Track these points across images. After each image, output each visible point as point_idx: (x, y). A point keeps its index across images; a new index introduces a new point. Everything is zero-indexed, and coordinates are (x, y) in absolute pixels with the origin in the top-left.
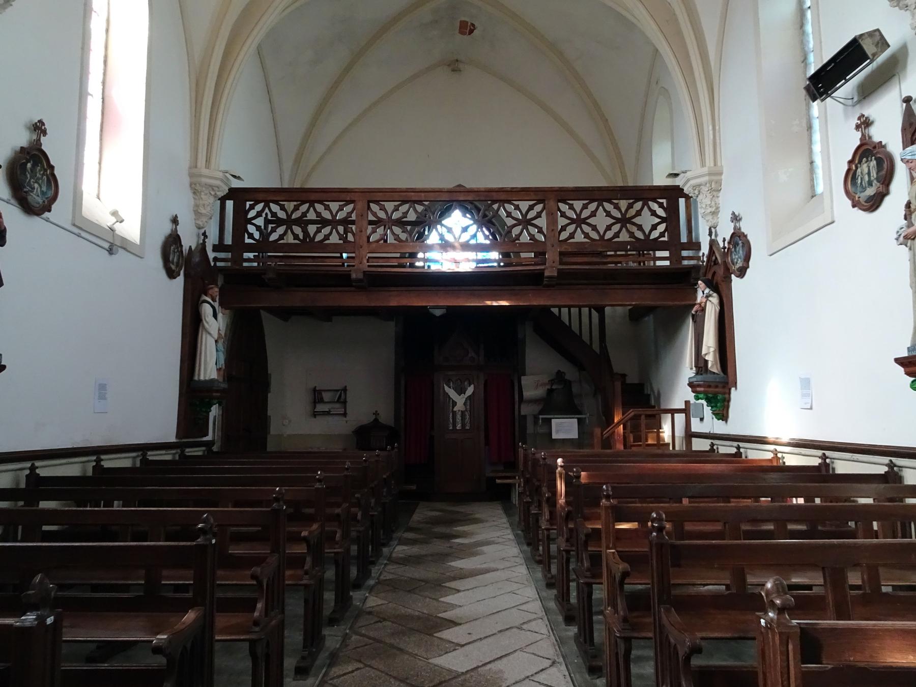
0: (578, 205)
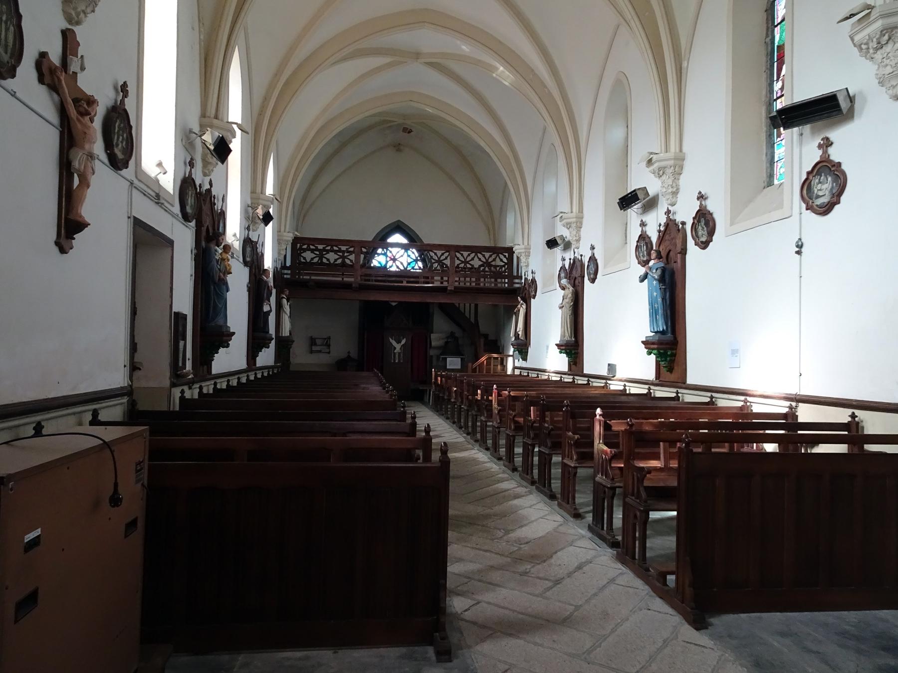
0: (465, 254)
